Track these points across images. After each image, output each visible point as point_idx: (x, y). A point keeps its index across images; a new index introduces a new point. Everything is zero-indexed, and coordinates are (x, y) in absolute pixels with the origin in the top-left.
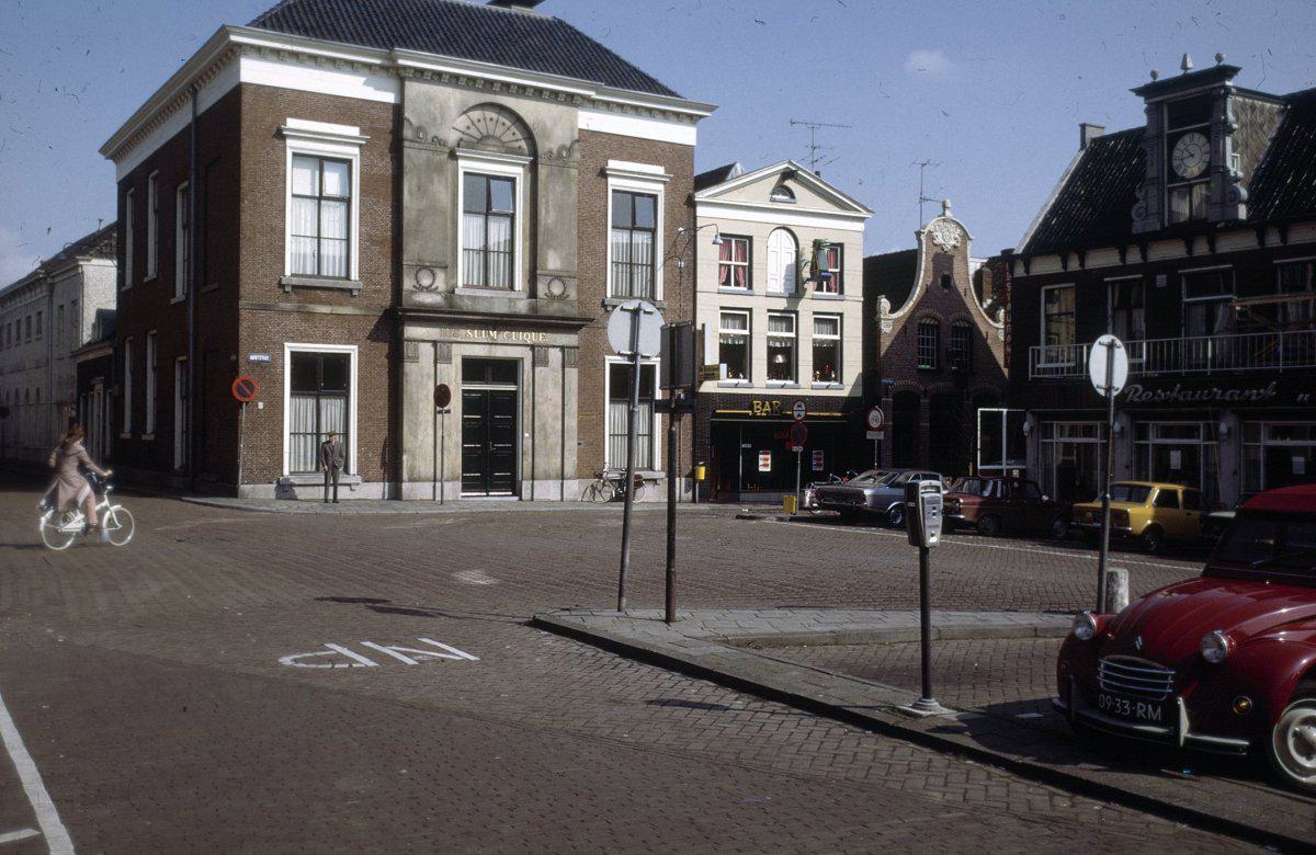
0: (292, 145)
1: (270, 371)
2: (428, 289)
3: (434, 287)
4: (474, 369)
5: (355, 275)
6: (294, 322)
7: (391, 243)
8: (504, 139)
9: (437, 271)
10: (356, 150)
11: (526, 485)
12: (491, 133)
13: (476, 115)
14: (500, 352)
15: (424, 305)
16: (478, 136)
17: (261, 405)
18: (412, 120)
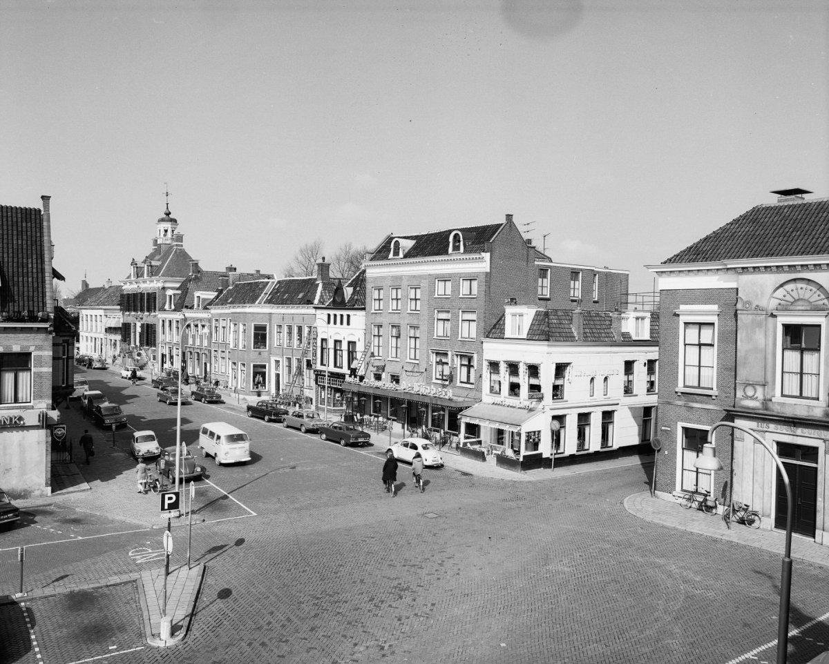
0: (683, 319)
1: (670, 435)
2: (752, 398)
6: (683, 411)
7: (730, 369)
8: (811, 300)
9: (757, 387)
11: (818, 532)
12: (797, 297)
13: (789, 287)
15: (749, 408)
16: (792, 300)
17: (666, 453)
18: (743, 298)
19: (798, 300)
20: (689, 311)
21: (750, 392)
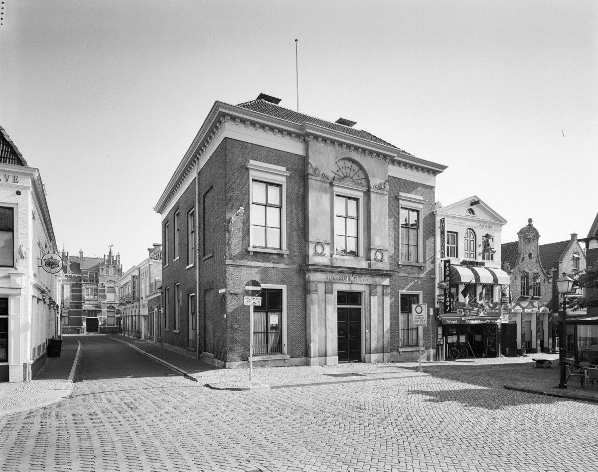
4: (343, 297)
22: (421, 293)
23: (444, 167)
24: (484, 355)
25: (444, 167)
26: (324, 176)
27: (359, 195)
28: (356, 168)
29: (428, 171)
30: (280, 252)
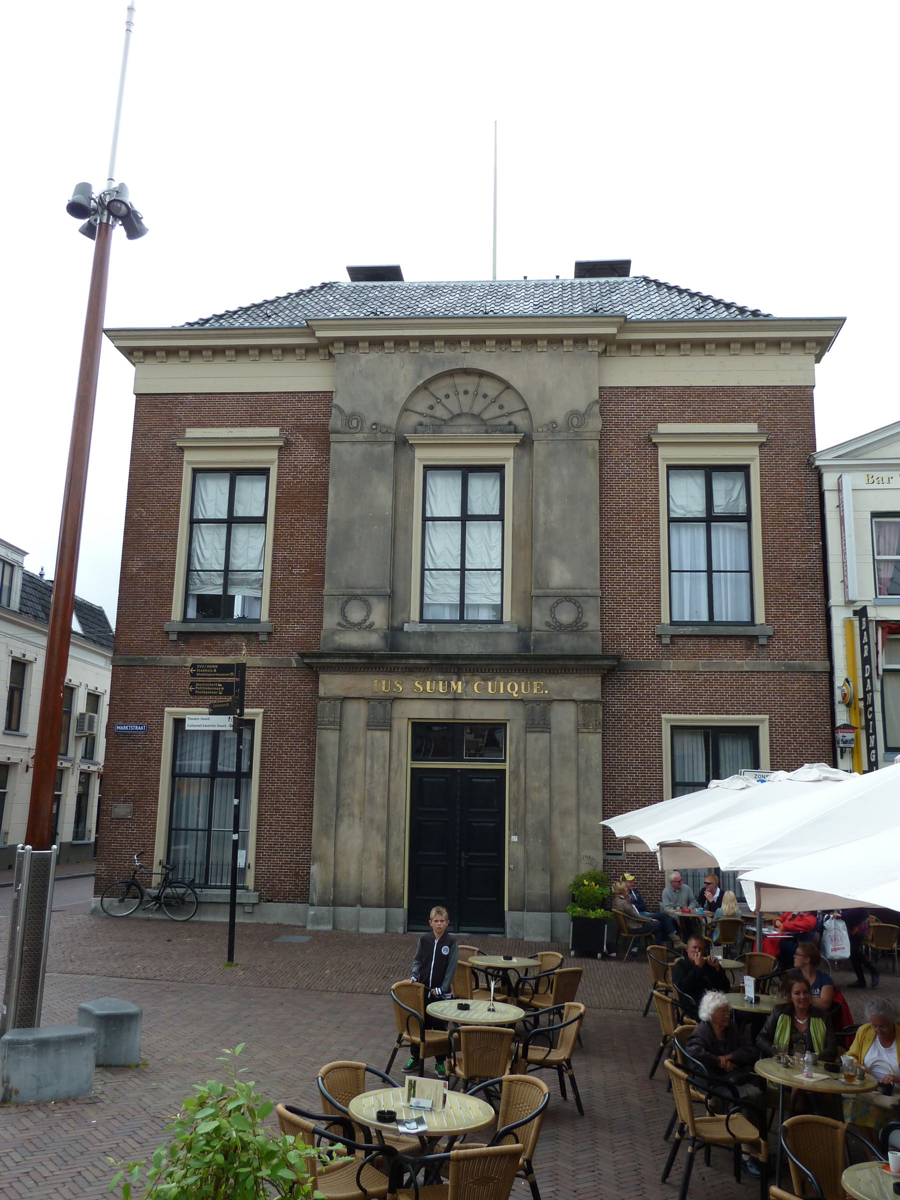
0: (667, 455)
2: (364, 626)
3: (367, 623)
4: (429, 738)
5: (760, 618)
8: (486, 416)
9: (374, 601)
10: (755, 452)
12: (456, 411)
14: (471, 712)
19: (459, 415)
20: (681, 439)
21: (356, 614)
22: (763, 722)
23: (837, 323)
24: (839, 944)
25: (837, 323)
26: (376, 426)
27: (505, 455)
28: (468, 383)
29: (800, 344)
30: (750, 631)
